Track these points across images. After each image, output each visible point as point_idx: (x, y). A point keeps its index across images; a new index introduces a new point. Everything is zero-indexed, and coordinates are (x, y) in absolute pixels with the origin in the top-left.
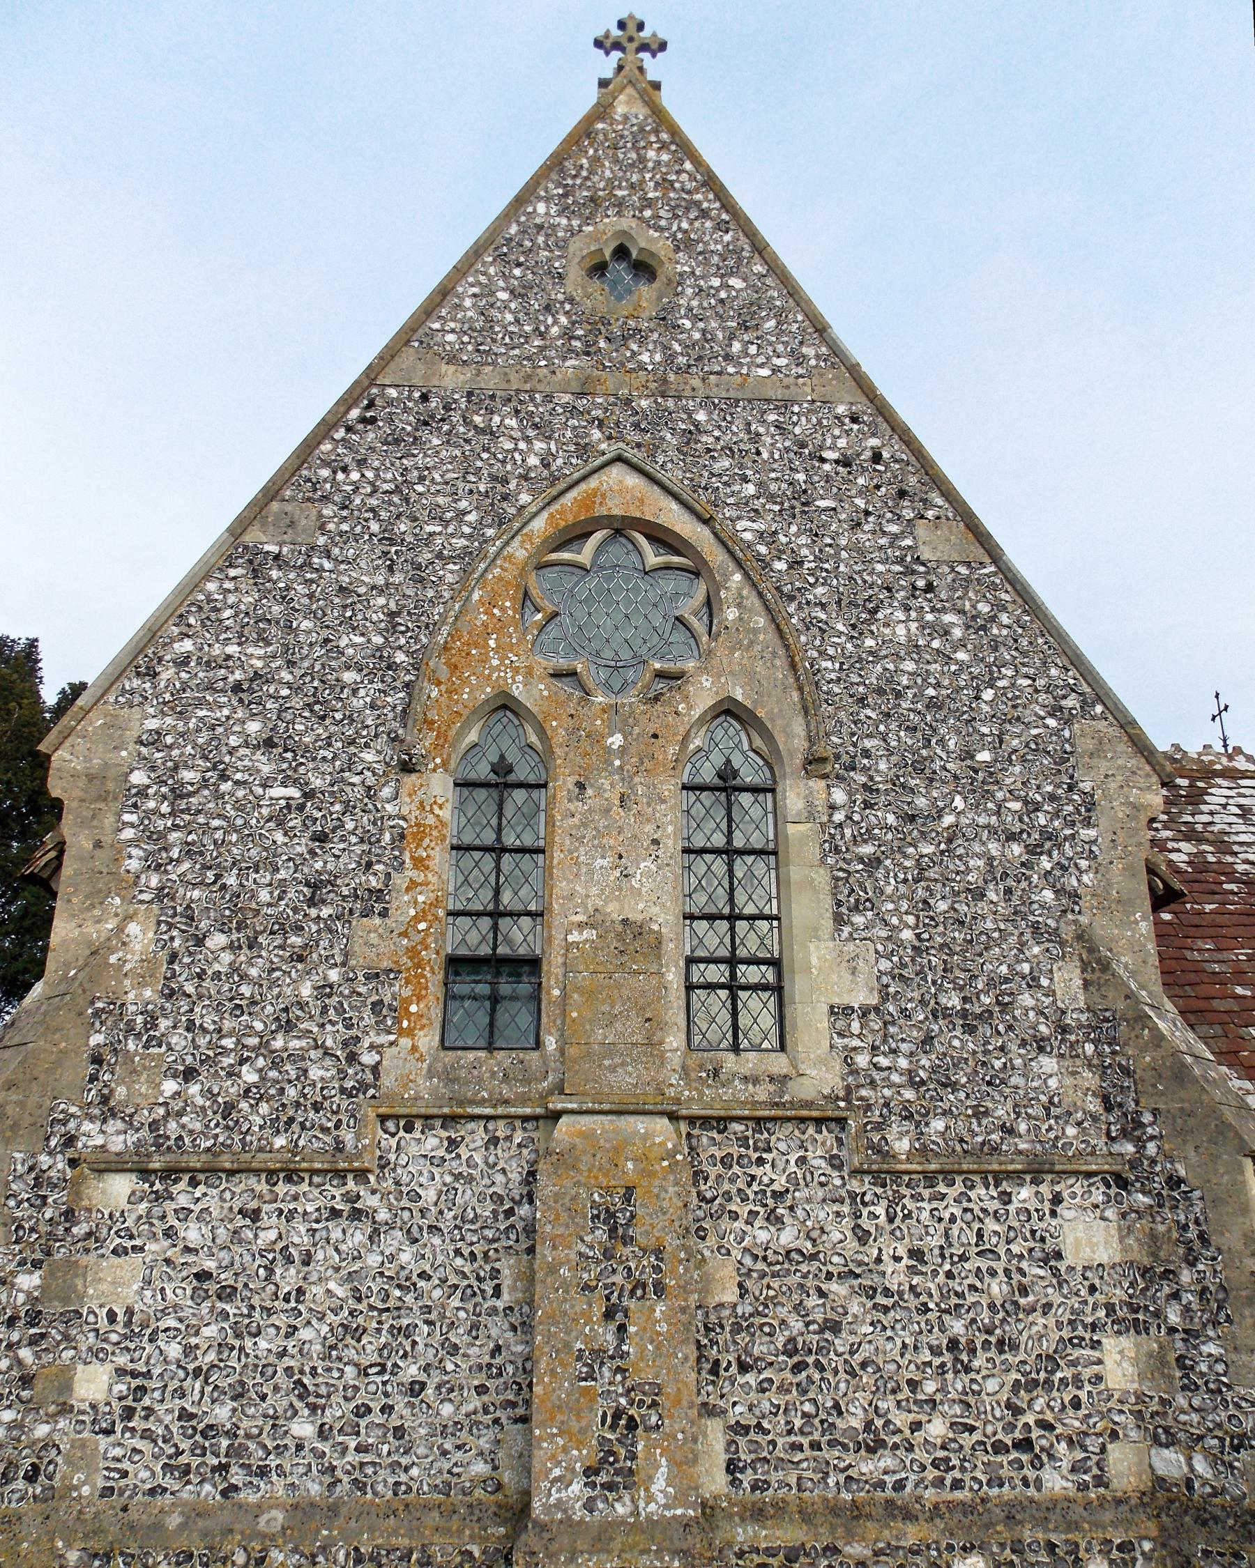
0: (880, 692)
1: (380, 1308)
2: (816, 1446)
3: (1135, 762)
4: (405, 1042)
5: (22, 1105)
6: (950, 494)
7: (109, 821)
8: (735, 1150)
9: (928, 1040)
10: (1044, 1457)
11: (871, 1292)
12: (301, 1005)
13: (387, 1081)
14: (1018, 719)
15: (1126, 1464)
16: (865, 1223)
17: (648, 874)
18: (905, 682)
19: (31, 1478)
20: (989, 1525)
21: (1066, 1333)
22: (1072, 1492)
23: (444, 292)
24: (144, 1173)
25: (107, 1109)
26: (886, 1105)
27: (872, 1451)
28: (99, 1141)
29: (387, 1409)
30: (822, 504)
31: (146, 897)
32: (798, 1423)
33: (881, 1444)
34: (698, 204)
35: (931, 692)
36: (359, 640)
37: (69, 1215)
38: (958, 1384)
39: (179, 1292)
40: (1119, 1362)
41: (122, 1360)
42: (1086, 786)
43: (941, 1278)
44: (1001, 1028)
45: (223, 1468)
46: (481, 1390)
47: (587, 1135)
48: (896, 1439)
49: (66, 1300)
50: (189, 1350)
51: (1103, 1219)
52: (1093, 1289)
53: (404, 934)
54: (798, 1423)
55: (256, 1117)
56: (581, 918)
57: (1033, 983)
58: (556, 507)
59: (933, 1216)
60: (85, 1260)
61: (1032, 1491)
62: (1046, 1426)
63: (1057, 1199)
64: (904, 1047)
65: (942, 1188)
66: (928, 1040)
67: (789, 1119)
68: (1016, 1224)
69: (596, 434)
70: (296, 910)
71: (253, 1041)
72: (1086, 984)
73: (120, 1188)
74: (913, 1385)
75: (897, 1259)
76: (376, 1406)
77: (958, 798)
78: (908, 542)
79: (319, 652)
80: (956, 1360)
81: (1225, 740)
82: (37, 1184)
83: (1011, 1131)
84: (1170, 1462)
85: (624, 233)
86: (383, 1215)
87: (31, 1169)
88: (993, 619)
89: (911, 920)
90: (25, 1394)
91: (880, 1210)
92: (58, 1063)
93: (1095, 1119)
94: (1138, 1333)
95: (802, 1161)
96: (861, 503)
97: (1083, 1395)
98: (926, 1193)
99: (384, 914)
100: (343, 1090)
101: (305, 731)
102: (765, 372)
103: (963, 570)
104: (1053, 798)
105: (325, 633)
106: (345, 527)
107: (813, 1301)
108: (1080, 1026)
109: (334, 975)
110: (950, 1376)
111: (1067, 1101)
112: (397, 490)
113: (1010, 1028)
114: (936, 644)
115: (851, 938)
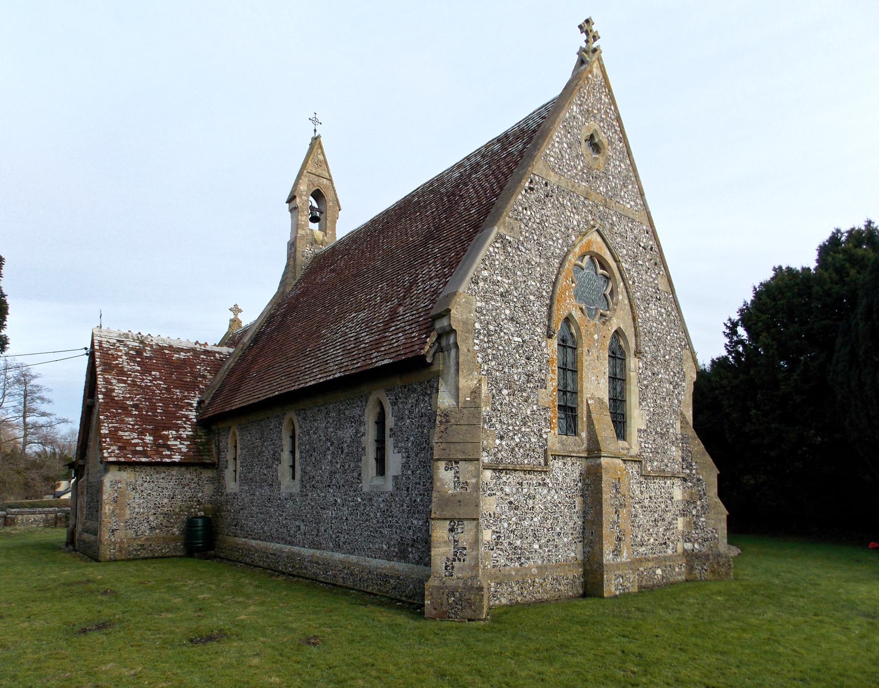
1: (551, 511)
3: (693, 364)
6: (666, 268)
11: (642, 507)
12: (528, 417)
13: (549, 444)
15: (679, 547)
31: (484, 373)
39: (506, 507)
40: (680, 523)
45: (520, 558)
46: (572, 534)
72: (681, 427)
73: (488, 474)
83: (667, 466)
84: (688, 546)
85: (596, 131)
86: (550, 485)
99: (546, 388)
105: (525, 279)
109: (535, 407)
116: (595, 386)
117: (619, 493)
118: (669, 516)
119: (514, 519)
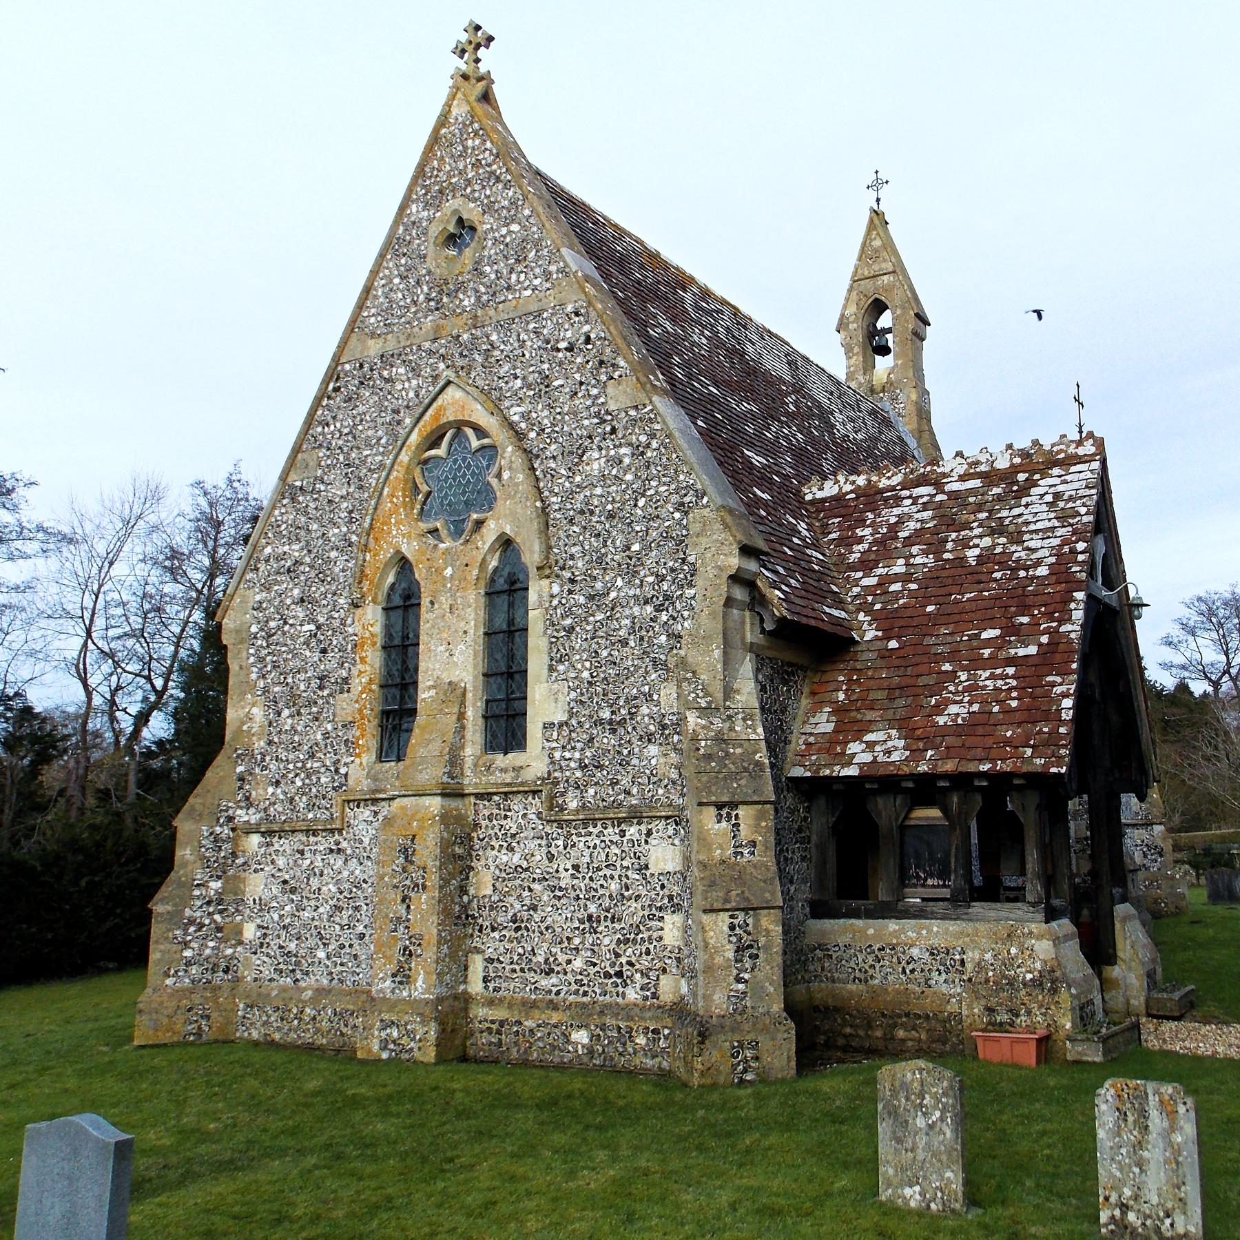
0: (582, 512)
2: (522, 970)
4: (358, 761)
5: (203, 804)
7: (244, 654)
8: (495, 811)
9: (591, 740)
10: (628, 981)
11: (553, 889)
13: (351, 782)
14: (658, 517)
15: (670, 987)
16: (554, 851)
17: (462, 653)
18: (596, 503)
19: (226, 971)
20: (591, 1015)
21: (646, 913)
22: (640, 1001)
23: (367, 290)
24: (263, 834)
25: (248, 802)
26: (567, 781)
27: (547, 974)
28: (246, 818)
29: (351, 946)
30: (556, 383)
32: (516, 958)
33: (552, 970)
34: (493, 173)
35: (609, 507)
36: (336, 531)
37: (234, 855)
38: (590, 939)
39: (276, 889)
41: (258, 921)
42: (691, 559)
43: (587, 880)
44: (630, 729)
47: (403, 808)
48: (559, 968)
49: (236, 894)
50: (281, 916)
51: (673, 844)
52: (663, 887)
53: (357, 702)
54: (516, 958)
55: (302, 802)
56: (431, 683)
57: (649, 697)
58: (422, 423)
59: (586, 846)
60: (242, 874)
61: (620, 1000)
62: (630, 964)
63: (649, 833)
64: (579, 745)
65: (591, 829)
66: (591, 740)
67: (519, 792)
68: (627, 849)
69: (442, 366)
70: (315, 693)
71: (299, 765)
74: (569, 939)
75: (567, 870)
76: (347, 944)
77: (619, 579)
78: (602, 400)
79: (321, 541)
80: (591, 927)
81: (1080, 427)
82: (216, 841)
83: (628, 793)
86: (349, 852)
87: (211, 834)
88: (648, 446)
89: (588, 664)
90: (219, 935)
91: (560, 843)
92: (220, 782)
93: (674, 783)
94: (260, 899)
95: (525, 815)
96: (577, 376)
97: (651, 947)
98: (583, 832)
99: (348, 692)
100: (334, 788)
101: (317, 590)
102: (528, 293)
103: (633, 413)
104: (673, 570)
106: (329, 462)
107: (526, 893)
108: (673, 724)
110: (587, 935)
111: (660, 772)
112: (351, 432)
113: (634, 728)
114: (614, 472)
115: (557, 680)
116: (452, 657)
117: (412, 862)
118: (633, 911)
119: (288, 908)
